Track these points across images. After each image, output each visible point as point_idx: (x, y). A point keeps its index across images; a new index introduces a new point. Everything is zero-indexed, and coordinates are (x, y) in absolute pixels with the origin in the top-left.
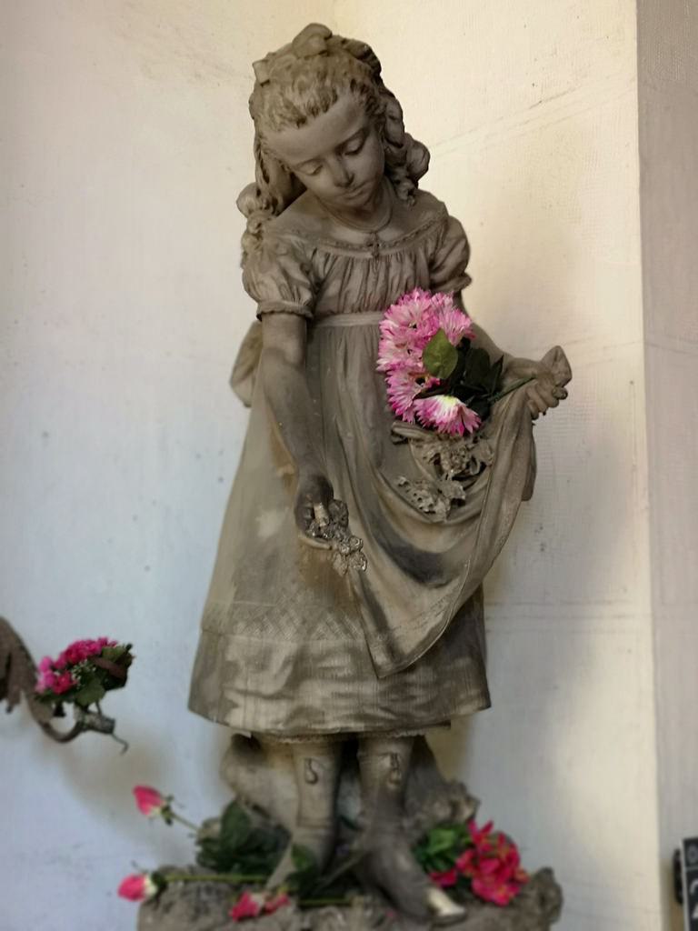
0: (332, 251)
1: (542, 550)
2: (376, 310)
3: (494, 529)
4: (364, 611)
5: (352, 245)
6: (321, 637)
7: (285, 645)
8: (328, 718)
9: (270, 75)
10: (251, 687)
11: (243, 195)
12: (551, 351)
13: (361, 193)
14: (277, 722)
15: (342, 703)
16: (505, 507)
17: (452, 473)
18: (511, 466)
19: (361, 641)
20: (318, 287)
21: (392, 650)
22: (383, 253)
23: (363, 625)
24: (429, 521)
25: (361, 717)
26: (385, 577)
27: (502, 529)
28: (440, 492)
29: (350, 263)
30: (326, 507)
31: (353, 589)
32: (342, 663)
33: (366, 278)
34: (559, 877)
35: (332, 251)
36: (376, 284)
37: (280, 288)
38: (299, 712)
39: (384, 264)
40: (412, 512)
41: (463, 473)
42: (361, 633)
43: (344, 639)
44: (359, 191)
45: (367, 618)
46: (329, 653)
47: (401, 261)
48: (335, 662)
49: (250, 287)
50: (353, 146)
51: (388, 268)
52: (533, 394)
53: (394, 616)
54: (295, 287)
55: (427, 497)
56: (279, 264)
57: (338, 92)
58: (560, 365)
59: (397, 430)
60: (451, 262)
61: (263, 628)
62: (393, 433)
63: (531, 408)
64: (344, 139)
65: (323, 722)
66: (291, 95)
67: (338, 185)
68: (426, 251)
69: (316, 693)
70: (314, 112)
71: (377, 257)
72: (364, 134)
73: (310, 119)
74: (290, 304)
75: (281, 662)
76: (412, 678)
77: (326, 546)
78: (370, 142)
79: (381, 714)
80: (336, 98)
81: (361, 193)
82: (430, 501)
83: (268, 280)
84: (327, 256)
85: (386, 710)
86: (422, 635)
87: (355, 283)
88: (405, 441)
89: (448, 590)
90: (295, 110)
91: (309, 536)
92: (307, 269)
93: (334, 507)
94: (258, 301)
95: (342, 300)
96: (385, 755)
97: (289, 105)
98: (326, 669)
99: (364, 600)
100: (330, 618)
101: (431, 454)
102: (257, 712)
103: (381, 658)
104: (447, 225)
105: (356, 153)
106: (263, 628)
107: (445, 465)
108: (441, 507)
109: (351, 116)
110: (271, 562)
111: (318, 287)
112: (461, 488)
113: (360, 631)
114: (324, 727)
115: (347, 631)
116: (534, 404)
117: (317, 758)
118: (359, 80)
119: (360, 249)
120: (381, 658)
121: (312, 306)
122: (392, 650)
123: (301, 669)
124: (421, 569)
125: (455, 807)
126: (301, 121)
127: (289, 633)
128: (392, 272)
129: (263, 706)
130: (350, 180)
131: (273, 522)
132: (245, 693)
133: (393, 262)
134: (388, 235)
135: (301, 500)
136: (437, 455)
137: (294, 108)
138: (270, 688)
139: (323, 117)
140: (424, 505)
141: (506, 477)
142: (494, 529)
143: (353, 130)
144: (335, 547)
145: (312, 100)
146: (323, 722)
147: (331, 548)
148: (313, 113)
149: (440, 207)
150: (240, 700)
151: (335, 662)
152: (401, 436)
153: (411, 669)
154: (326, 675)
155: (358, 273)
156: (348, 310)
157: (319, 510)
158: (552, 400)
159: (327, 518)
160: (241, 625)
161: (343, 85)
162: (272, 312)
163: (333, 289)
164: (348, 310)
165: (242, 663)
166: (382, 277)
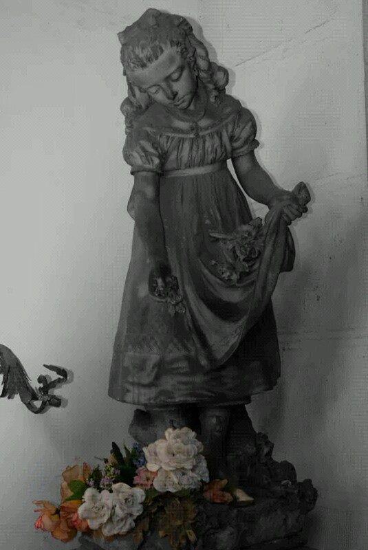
0: (171, 135)
1: (318, 300)
2: (199, 166)
3: (264, 288)
4: (194, 337)
5: (182, 130)
6: (171, 351)
7: (154, 357)
8: (176, 396)
9: (129, 37)
10: (136, 380)
11: (123, 105)
12: (297, 185)
13: (183, 102)
14: (150, 399)
15: (183, 387)
16: (270, 276)
17: (242, 258)
18: (273, 252)
19: (193, 353)
20: (163, 157)
21: (210, 357)
22: (201, 134)
23: (194, 344)
24: (229, 284)
25: (191, 395)
26: (206, 317)
27: (269, 288)
28: (235, 268)
29: (182, 140)
30: (164, 280)
31: (188, 325)
32: (183, 365)
33: (191, 148)
34: (315, 484)
35: (171, 135)
36: (197, 151)
37: (141, 157)
38: (162, 393)
39: (202, 140)
40: (218, 280)
41: (248, 257)
42: (193, 349)
43: (183, 352)
44: (181, 100)
45: (196, 340)
46: (177, 360)
47: (212, 137)
48: (179, 365)
49: (127, 158)
50: (175, 76)
51: (204, 142)
52: (286, 210)
53: (213, 339)
54: (149, 157)
55: (227, 271)
56: (140, 144)
57: (164, 48)
58: (303, 194)
59: (211, 234)
60: (244, 135)
61: (142, 347)
62: (211, 236)
63: (285, 218)
64: (169, 74)
65: (173, 398)
66: (138, 51)
67: (169, 98)
68: (227, 131)
69: (168, 383)
70: (149, 60)
71: (197, 135)
72: (181, 69)
73: (148, 64)
74: (147, 166)
75: (151, 366)
76: (223, 373)
77: (163, 300)
78: (185, 73)
79: (206, 393)
80: (162, 51)
81: (183, 102)
82: (228, 274)
83: (135, 154)
84: (168, 138)
85: (209, 391)
86: (226, 349)
87: (185, 154)
88: (218, 240)
89: (240, 323)
90: (141, 60)
91: (154, 295)
92: (156, 145)
93: (169, 279)
94: (132, 165)
95: (179, 161)
96: (213, 417)
97: (137, 57)
98: (173, 369)
99: (194, 330)
100: (175, 340)
101: (230, 247)
102: (139, 394)
103: (204, 362)
104: (244, 116)
105: (177, 80)
106: (142, 347)
107: (238, 253)
108: (235, 277)
109: (171, 60)
110: (146, 311)
111: (163, 157)
112: (247, 266)
113: (194, 346)
114: (173, 400)
115: (186, 348)
116: (287, 216)
117: (177, 420)
118: (175, 40)
119: (187, 132)
120: (204, 362)
121: (162, 164)
122: (210, 357)
123: (162, 369)
124: (224, 311)
125: (259, 449)
126: (143, 66)
127: (155, 349)
128: (207, 144)
129: (143, 391)
130: (175, 95)
131: (143, 290)
132: (133, 384)
133: (208, 138)
134: (203, 123)
135: (151, 276)
136: (234, 247)
137: (139, 58)
138: (146, 381)
139: (154, 64)
140: (226, 275)
141: (271, 258)
142: (264, 288)
143: (173, 68)
144: (169, 301)
145: (149, 54)
146: (173, 398)
147: (166, 302)
148: (149, 60)
149: (237, 102)
150: (130, 388)
151: (179, 365)
152: (215, 238)
153: (223, 367)
154: (175, 372)
155: (187, 146)
156: (183, 167)
157: (160, 281)
158: (296, 213)
159: (164, 285)
160: (130, 347)
161: (166, 43)
162: (138, 171)
163: (173, 157)
164: (183, 167)
165: (131, 368)
166: (201, 146)
